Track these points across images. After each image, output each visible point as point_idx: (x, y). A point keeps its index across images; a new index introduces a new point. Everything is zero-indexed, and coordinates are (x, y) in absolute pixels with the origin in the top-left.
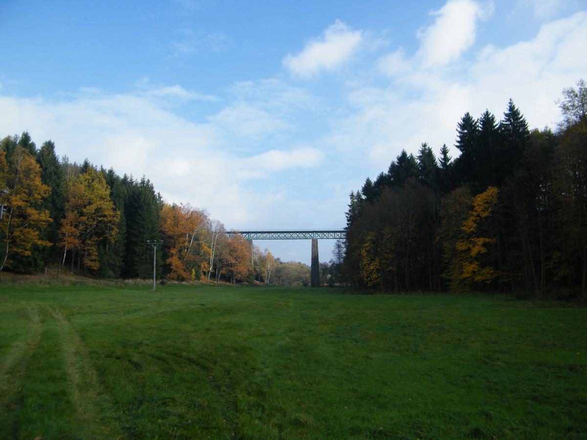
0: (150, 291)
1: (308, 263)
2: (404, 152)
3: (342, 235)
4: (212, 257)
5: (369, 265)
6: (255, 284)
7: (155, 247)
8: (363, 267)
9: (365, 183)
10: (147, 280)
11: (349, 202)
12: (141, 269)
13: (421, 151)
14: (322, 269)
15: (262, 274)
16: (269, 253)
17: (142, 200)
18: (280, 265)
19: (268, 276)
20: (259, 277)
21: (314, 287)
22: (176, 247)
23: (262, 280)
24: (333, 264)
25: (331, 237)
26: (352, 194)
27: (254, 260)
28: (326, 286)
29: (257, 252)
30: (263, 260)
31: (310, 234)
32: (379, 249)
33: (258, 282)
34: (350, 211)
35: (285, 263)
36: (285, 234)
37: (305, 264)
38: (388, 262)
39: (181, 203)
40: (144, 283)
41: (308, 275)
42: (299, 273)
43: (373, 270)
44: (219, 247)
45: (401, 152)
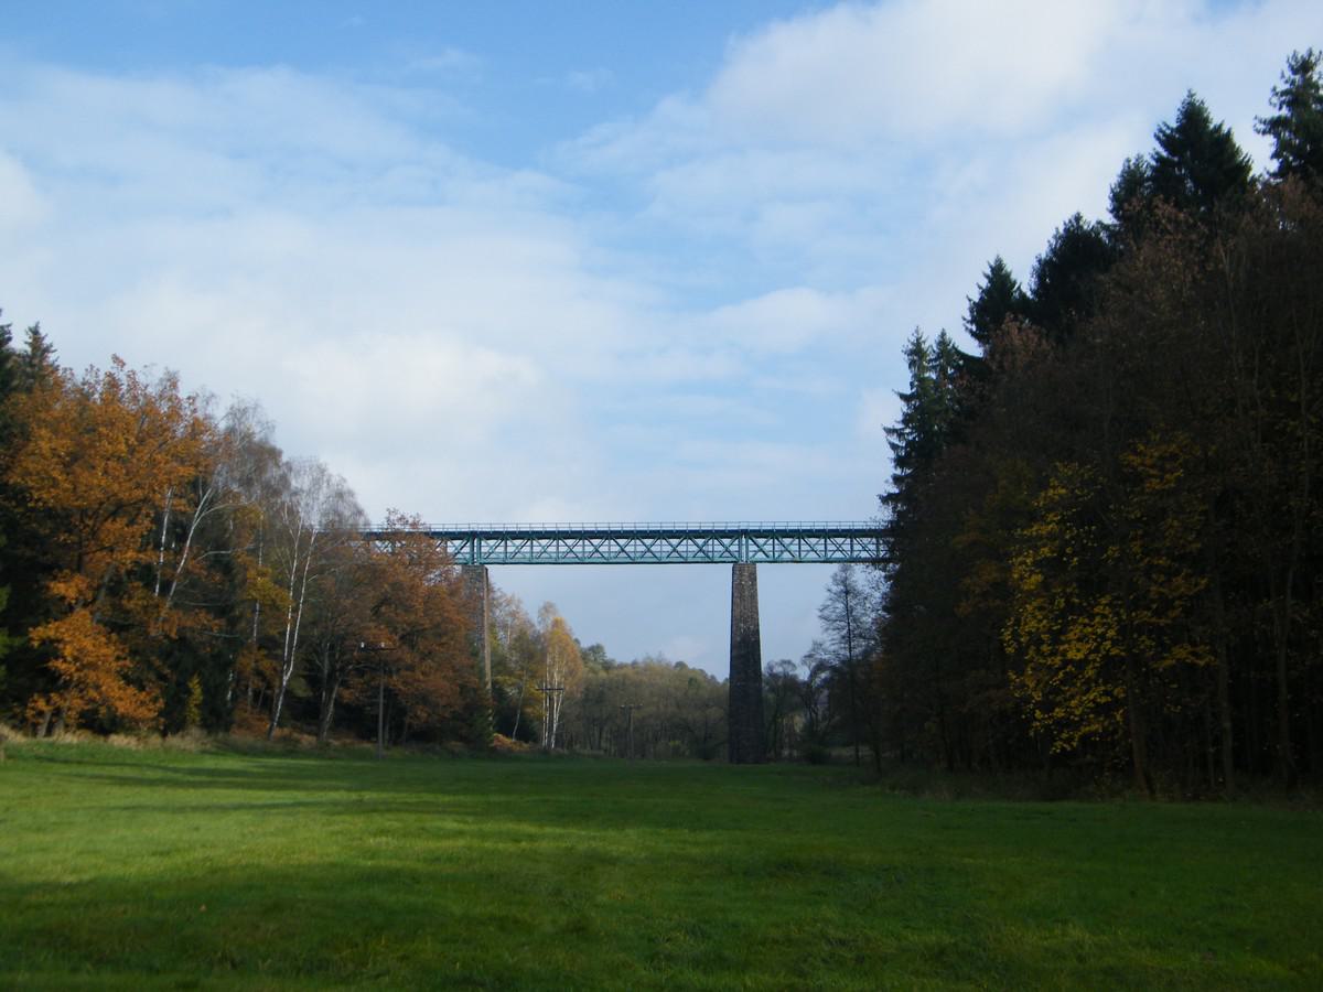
1: (719, 668)
2: (1191, 104)
3: (857, 547)
4: (291, 631)
5: (1056, 638)
6: (494, 749)
8: (1021, 651)
9: (985, 283)
11: (904, 380)
13: (1284, 93)
14: (772, 690)
15: (529, 710)
16: (557, 623)
18: (603, 674)
19: (551, 714)
20: (516, 721)
21: (739, 761)
23: (527, 733)
24: (821, 666)
25: (812, 555)
26: (918, 343)
27: (494, 653)
28: (790, 758)
29: (509, 620)
30: (532, 650)
31: (726, 541)
32: (1113, 550)
33: (508, 741)
34: (907, 420)
35: (621, 666)
36: (622, 542)
37: (702, 671)
38: (1162, 622)
39: (116, 359)
41: (715, 713)
42: (678, 706)
43: (1081, 665)
44: (328, 582)
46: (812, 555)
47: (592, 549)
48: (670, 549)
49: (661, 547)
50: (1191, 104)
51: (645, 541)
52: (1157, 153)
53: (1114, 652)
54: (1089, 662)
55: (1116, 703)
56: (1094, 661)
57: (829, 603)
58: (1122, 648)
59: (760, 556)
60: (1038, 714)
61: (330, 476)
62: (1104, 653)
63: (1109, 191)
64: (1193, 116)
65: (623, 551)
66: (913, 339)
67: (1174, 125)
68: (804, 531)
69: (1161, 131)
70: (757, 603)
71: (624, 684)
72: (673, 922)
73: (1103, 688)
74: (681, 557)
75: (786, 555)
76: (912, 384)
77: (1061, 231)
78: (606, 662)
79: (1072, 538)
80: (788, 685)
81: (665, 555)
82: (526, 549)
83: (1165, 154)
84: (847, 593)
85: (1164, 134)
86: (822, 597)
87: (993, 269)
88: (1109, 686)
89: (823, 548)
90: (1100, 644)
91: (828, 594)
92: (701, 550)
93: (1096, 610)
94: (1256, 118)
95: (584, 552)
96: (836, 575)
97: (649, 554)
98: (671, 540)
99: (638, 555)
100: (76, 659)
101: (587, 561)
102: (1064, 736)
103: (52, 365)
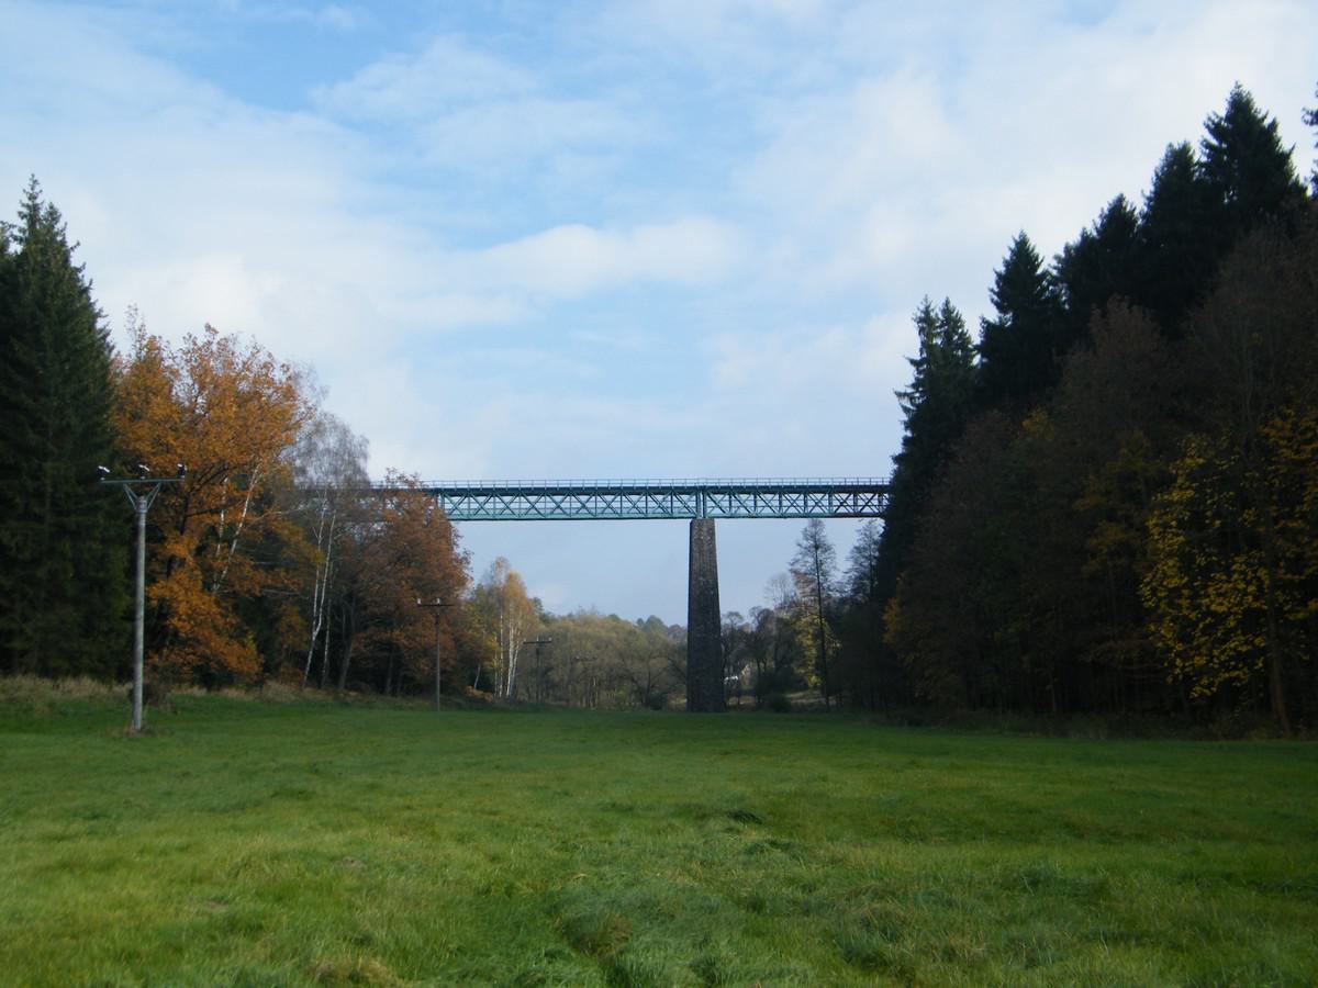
0: (115, 733)
1: (676, 614)
2: (1238, 95)
4: (320, 592)
7: (143, 501)
10: (70, 684)
12: (28, 629)
16: (510, 578)
17: (28, 297)
22: (192, 523)
25: (767, 511)
26: (927, 311)
30: (501, 599)
39: (208, 328)
40: (56, 695)
45: (1228, 96)
46: (743, 511)
47: (502, 506)
48: (553, 505)
49: (545, 504)
50: (1238, 95)
51: (530, 498)
52: (1205, 140)
53: (1255, 605)
54: (1231, 613)
55: (1259, 652)
56: (1236, 613)
57: (800, 557)
58: (1263, 602)
59: (717, 511)
60: (1178, 662)
61: (353, 437)
62: (1246, 606)
63: (1153, 175)
64: (1240, 107)
65: (558, 507)
66: (922, 308)
67: (1223, 113)
68: (761, 487)
69: (1209, 119)
70: (715, 556)
71: (565, 636)
72: (318, 878)
73: (1242, 638)
74: (565, 513)
75: (743, 511)
76: (921, 351)
77: (1106, 212)
78: (544, 615)
79: (1213, 503)
80: (738, 634)
81: (574, 511)
82: (464, 506)
83: (1214, 142)
84: (817, 547)
85: (1213, 123)
86: (793, 552)
87: (1017, 244)
88: (1250, 636)
89: (777, 503)
90: (1242, 598)
91: (799, 548)
92: (609, 506)
93: (1234, 567)
94: (1304, 109)
95: (469, 509)
96: (806, 530)
97: (559, 511)
98: (632, 497)
99: (523, 511)
100: (190, 617)
101: (600, 516)
102: (1205, 681)
103: (101, 330)
